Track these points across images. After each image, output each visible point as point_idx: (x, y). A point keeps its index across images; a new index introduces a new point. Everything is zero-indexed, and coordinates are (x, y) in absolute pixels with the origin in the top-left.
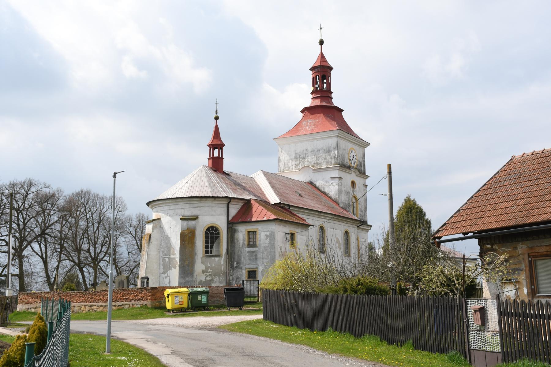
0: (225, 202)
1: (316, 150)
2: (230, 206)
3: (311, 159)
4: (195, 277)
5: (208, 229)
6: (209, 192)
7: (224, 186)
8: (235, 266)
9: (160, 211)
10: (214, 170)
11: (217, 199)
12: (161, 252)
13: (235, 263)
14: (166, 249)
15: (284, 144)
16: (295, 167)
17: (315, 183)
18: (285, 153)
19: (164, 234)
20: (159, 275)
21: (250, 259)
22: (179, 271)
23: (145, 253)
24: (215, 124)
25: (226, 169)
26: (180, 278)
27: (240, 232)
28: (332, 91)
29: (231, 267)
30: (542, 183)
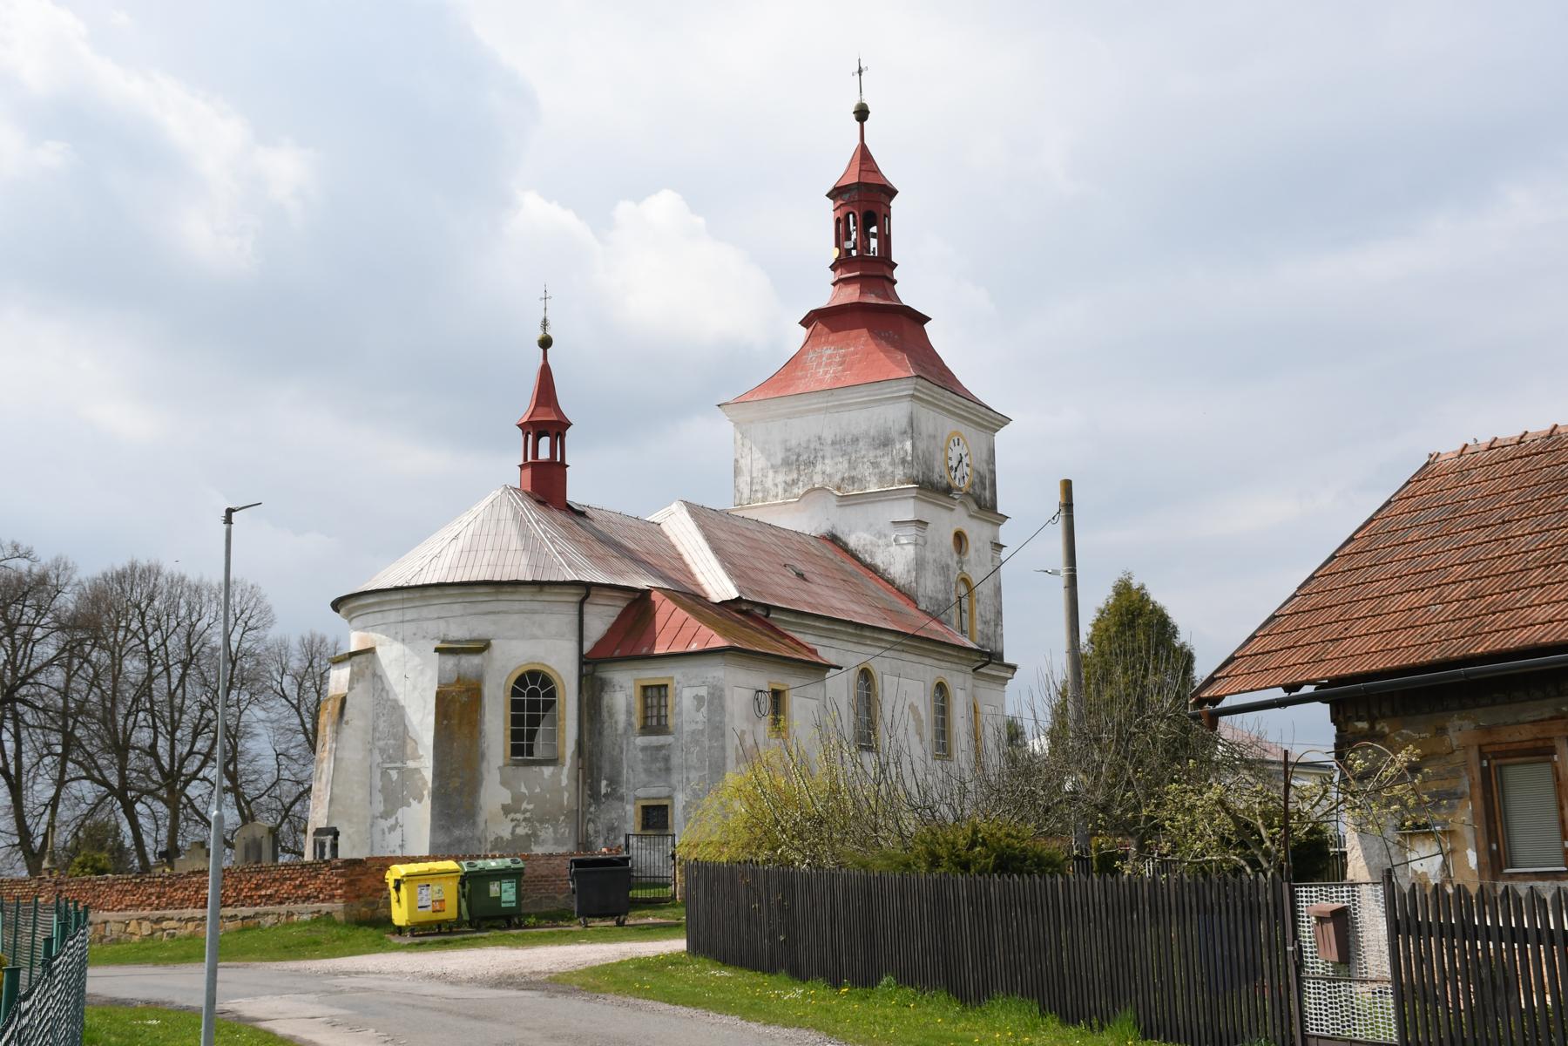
0: (573, 597)
1: (848, 438)
2: (587, 608)
3: (831, 468)
4: (482, 826)
5: (520, 681)
7: (569, 548)
8: (603, 791)
9: (373, 627)
11: (547, 589)
12: (376, 752)
13: (604, 783)
14: (392, 742)
15: (752, 422)
16: (785, 491)
17: (844, 538)
18: (754, 449)
19: (384, 694)
20: (369, 821)
23: (326, 754)
24: (540, 362)
27: (618, 688)
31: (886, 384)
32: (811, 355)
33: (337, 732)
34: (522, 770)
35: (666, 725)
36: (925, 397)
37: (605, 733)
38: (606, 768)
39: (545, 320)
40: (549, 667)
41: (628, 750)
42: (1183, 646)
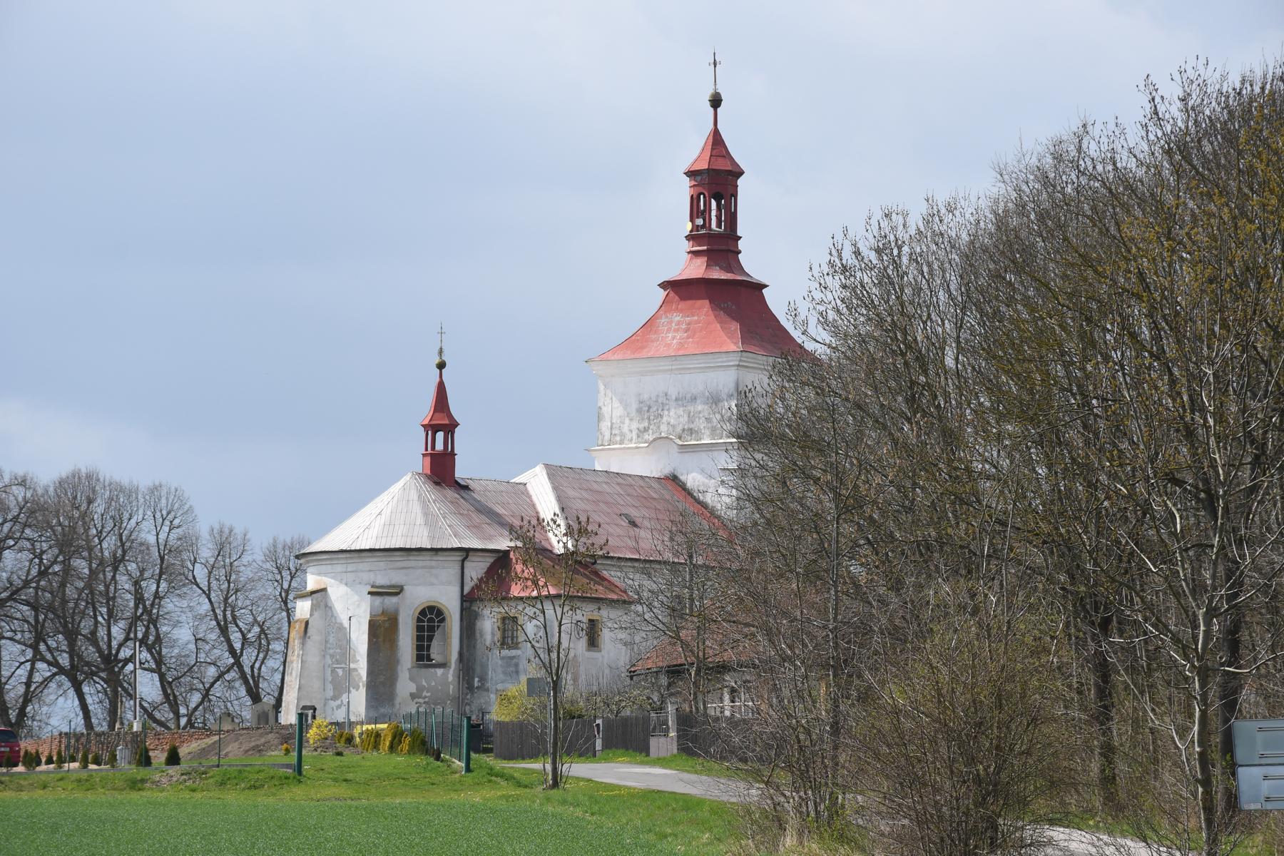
0: (458, 557)
1: (689, 396)
2: (467, 564)
3: (674, 417)
4: (398, 706)
5: (423, 613)
6: (425, 538)
7: (453, 520)
8: (476, 685)
9: (325, 574)
10: (437, 483)
11: (440, 553)
12: (328, 657)
13: (476, 679)
14: (339, 651)
15: (613, 376)
16: (638, 437)
17: (683, 478)
18: (614, 398)
19: (333, 619)
20: (323, 701)
22: (367, 694)
23: (295, 658)
24: (438, 379)
25: (460, 473)
26: (367, 708)
28: (739, 234)
29: (468, 688)
31: (717, 355)
32: (663, 320)
33: (303, 644)
34: (423, 670)
36: (751, 365)
37: (478, 647)
38: (478, 670)
39: (441, 349)
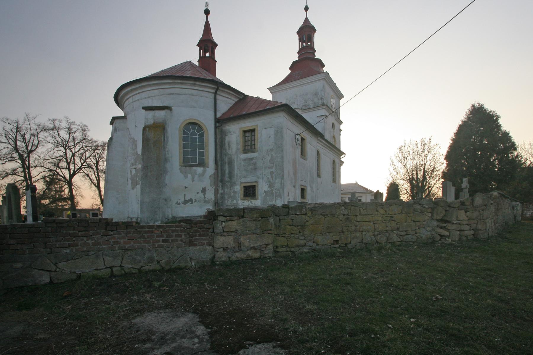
21: (246, 170)
27: (232, 133)
30: (205, 229)
35: (254, 148)
39: (207, 3)
40: (200, 122)
41: (237, 161)
42: (455, 135)
